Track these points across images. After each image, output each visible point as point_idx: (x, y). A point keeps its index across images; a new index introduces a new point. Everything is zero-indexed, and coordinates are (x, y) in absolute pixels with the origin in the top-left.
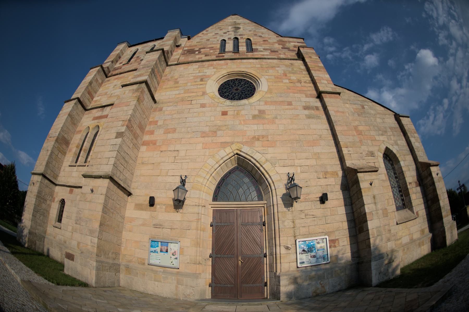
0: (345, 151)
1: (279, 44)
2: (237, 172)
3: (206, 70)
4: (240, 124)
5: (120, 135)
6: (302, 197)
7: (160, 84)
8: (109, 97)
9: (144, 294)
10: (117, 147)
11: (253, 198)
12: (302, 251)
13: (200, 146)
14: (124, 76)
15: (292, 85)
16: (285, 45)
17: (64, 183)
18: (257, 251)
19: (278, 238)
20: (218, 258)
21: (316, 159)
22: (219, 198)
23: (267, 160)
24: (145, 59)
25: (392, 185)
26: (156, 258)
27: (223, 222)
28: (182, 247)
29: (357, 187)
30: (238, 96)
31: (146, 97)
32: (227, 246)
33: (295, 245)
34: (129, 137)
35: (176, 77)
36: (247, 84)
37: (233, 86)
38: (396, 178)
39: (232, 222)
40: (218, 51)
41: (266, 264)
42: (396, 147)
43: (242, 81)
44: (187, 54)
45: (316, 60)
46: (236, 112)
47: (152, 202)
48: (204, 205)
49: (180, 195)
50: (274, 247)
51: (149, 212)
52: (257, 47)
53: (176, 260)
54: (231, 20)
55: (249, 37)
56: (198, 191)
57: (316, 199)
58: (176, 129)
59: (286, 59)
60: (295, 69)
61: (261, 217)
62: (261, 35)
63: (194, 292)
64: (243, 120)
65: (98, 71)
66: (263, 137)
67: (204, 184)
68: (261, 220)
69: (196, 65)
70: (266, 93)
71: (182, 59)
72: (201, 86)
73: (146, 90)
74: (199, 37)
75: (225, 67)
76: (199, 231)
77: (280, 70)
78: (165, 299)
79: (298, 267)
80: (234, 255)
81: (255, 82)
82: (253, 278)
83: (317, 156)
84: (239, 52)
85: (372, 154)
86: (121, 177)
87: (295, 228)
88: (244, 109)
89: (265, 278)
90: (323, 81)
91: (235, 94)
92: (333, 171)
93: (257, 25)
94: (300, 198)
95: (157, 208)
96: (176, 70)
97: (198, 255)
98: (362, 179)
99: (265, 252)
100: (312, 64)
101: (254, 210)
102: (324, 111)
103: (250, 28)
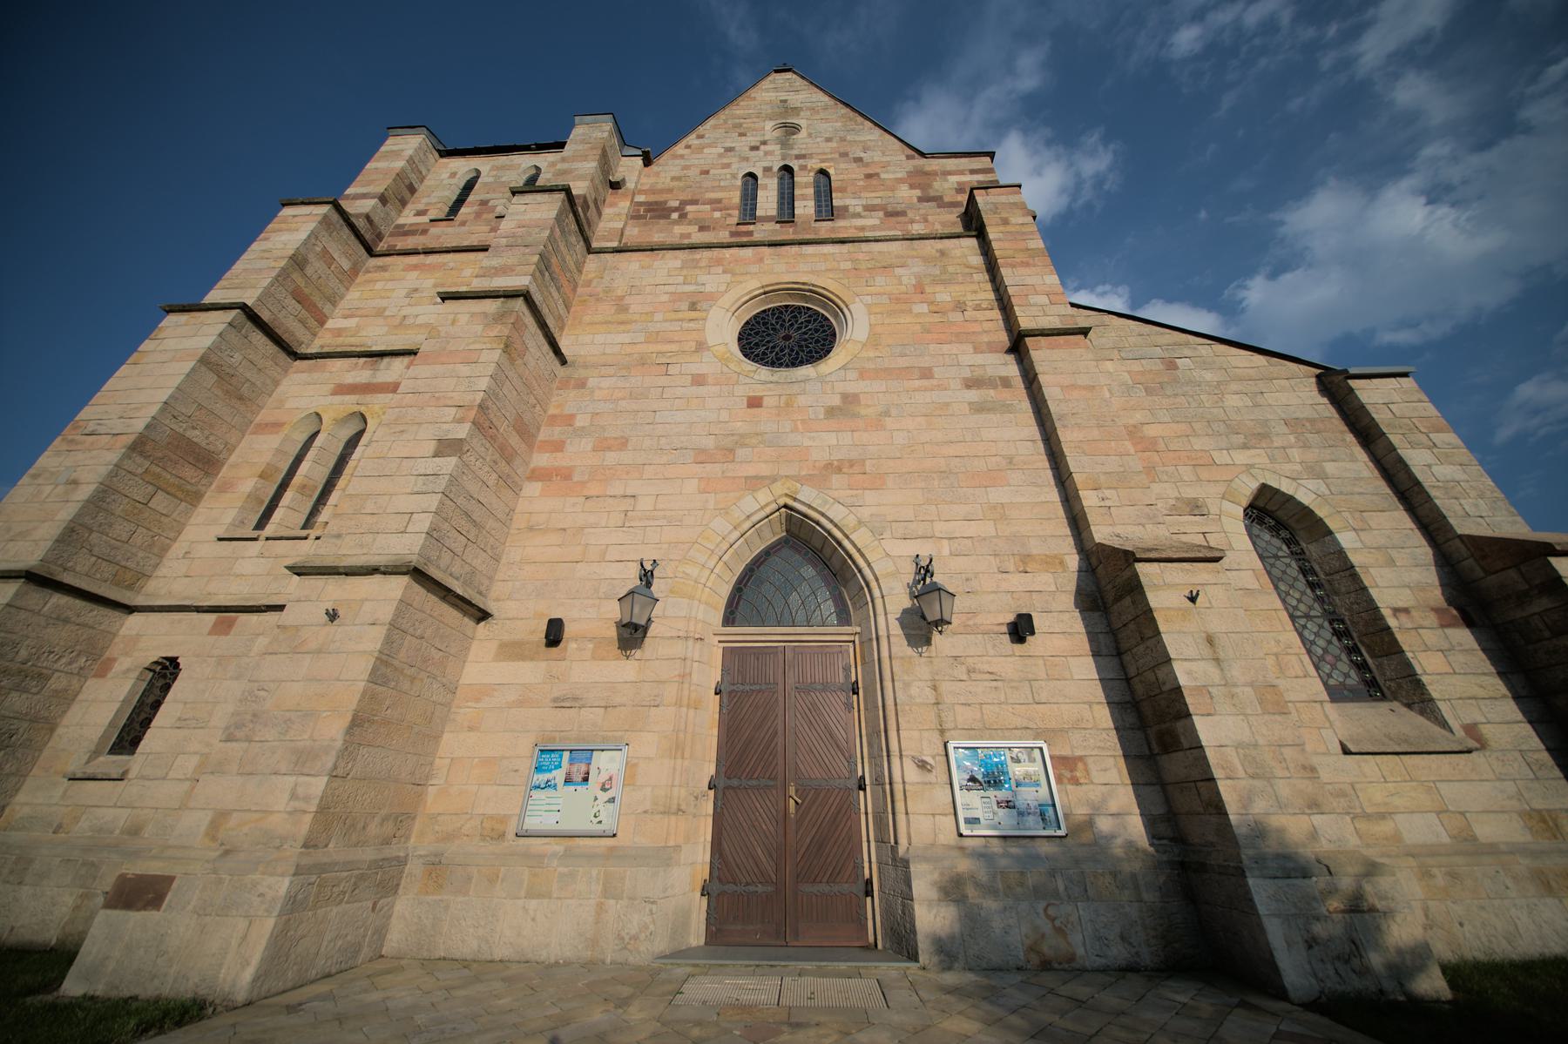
0: (1089, 499)
1: (912, 187)
2: (786, 552)
3: (703, 278)
4: (795, 430)
5: (446, 447)
6: (955, 621)
7: (572, 310)
8: (396, 327)
9: (475, 965)
10: (442, 483)
11: (824, 617)
12: (969, 780)
13: (691, 486)
14: (445, 264)
15: (937, 318)
16: (930, 186)
17: (185, 598)
18: (837, 769)
19: (895, 733)
20: (731, 791)
21: (995, 520)
22: (738, 616)
23: (860, 523)
24: (512, 214)
25: (1296, 608)
26: (548, 807)
27: (748, 681)
28: (635, 761)
29: (1133, 602)
30: (790, 355)
31: (531, 344)
32: (756, 751)
33: (945, 758)
34: (482, 454)
35: (619, 293)
36: (815, 320)
37: (778, 327)
38: (1312, 586)
39: (772, 681)
40: (735, 216)
41: (866, 813)
42: (1312, 484)
43: (800, 313)
44: (644, 217)
45: (1024, 229)
46: (783, 399)
47: (554, 634)
48: (699, 636)
49: (636, 610)
50: (885, 758)
51: (543, 665)
52: (848, 202)
53: (611, 806)
54: (772, 95)
55: (824, 165)
56: (686, 601)
57: (996, 629)
58: (627, 441)
59: (927, 239)
60: (951, 269)
61: (847, 669)
62: (862, 155)
63: (654, 922)
64: (803, 421)
65: (325, 220)
66: (852, 463)
67: (703, 581)
68: (848, 676)
69: (676, 258)
70: (864, 345)
71: (634, 234)
72: (692, 325)
73: (529, 319)
74: (675, 157)
75: (754, 268)
76: (685, 709)
77: (907, 277)
78: (549, 969)
79: (961, 835)
80: (775, 779)
81: (836, 316)
82: (829, 860)
83: (999, 513)
84: (796, 220)
85: (1196, 508)
86: (456, 569)
87: (940, 707)
88: (803, 393)
89: (866, 865)
90: (1033, 299)
91: (782, 350)
92: (1047, 553)
93: (852, 114)
94: (950, 623)
95: (569, 649)
96: (616, 268)
97: (677, 782)
98: (1155, 581)
99: (860, 774)
100: (1007, 245)
101: (827, 650)
102: (1026, 388)
103: (827, 128)
